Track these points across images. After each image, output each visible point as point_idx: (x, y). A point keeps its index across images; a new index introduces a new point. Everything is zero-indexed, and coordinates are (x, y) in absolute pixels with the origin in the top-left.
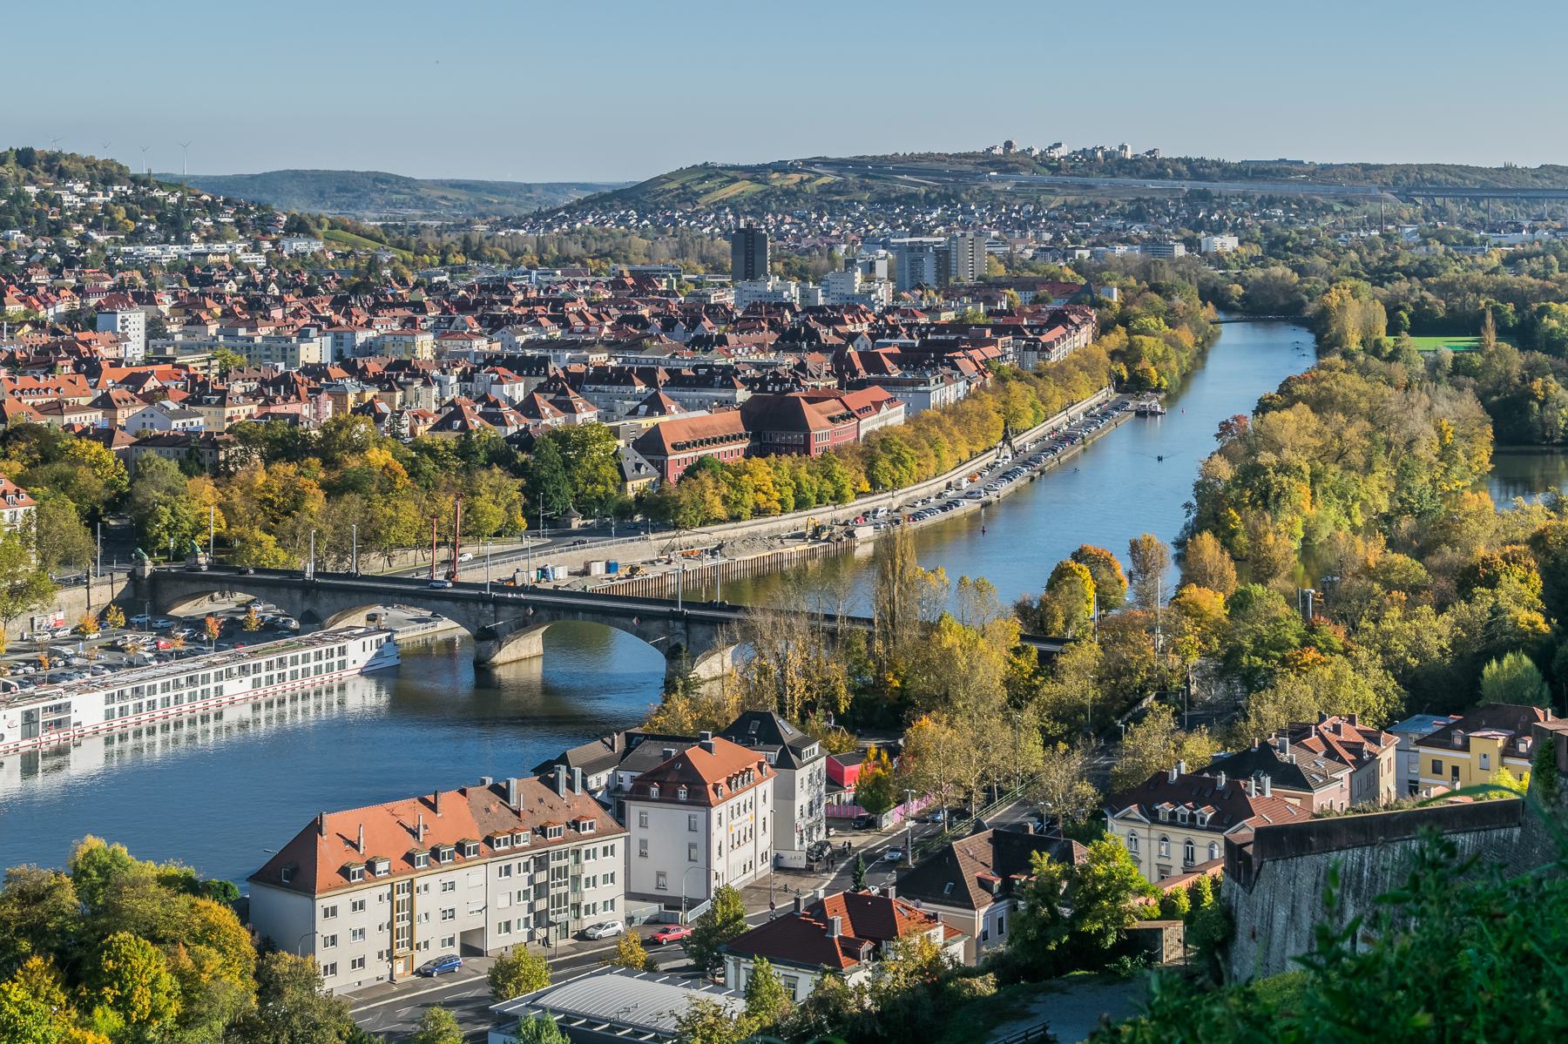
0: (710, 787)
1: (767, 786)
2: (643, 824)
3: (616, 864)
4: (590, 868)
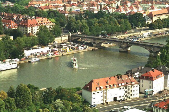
0: (153, 77)
1: (163, 77)
2: (143, 82)
3: (138, 88)
4: (133, 89)
